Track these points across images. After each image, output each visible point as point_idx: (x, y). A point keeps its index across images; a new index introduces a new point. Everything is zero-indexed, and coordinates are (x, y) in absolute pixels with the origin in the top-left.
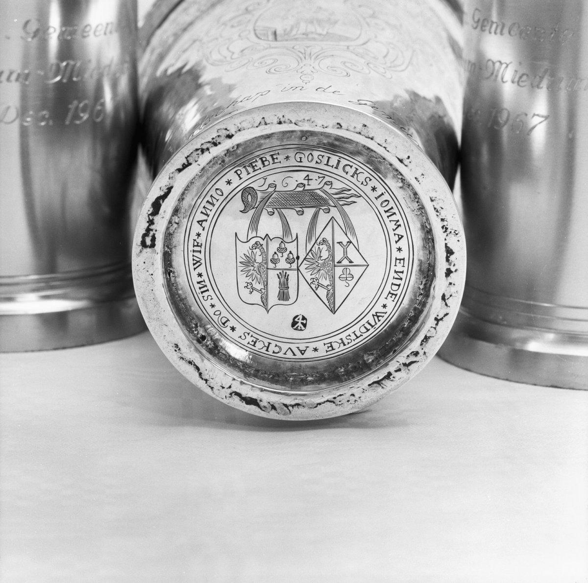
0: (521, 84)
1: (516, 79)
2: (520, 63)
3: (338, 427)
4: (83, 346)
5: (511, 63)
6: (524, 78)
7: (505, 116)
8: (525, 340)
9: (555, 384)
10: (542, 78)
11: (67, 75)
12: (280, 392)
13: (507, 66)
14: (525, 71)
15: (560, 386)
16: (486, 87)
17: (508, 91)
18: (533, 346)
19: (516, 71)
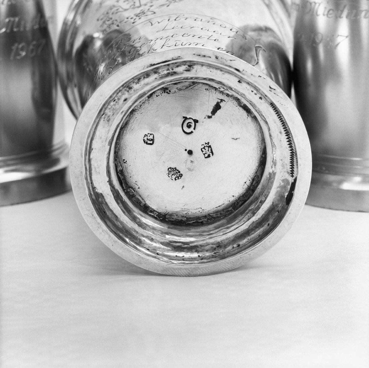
0: (329, 16)
1: (326, 13)
2: (328, 2)
3: (56, 104)
4: (18, 203)
5: (322, 2)
6: (331, 12)
7: (320, 37)
8: (341, 182)
9: (361, 210)
10: (342, 11)
11: (9, 27)
12: (127, 193)
13: (320, 4)
14: (331, 8)
15: (364, 210)
16: (307, 18)
17: (322, 23)
18: (346, 186)
19: (325, 8)
